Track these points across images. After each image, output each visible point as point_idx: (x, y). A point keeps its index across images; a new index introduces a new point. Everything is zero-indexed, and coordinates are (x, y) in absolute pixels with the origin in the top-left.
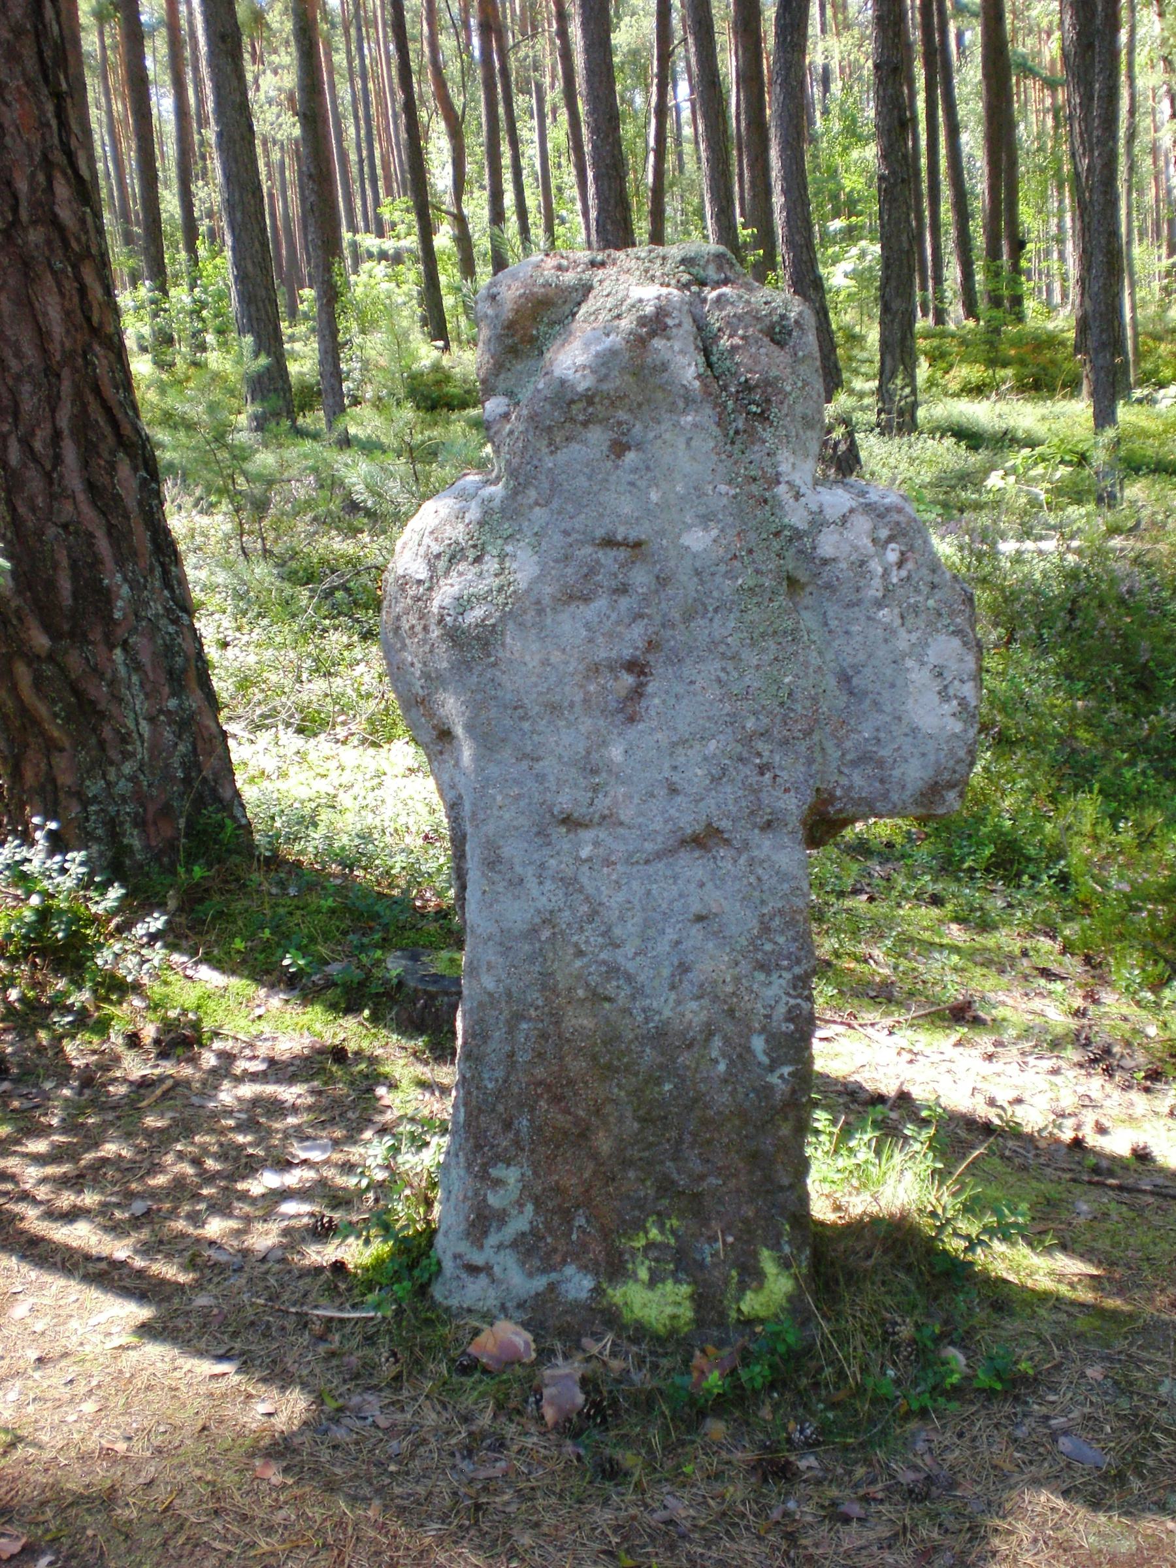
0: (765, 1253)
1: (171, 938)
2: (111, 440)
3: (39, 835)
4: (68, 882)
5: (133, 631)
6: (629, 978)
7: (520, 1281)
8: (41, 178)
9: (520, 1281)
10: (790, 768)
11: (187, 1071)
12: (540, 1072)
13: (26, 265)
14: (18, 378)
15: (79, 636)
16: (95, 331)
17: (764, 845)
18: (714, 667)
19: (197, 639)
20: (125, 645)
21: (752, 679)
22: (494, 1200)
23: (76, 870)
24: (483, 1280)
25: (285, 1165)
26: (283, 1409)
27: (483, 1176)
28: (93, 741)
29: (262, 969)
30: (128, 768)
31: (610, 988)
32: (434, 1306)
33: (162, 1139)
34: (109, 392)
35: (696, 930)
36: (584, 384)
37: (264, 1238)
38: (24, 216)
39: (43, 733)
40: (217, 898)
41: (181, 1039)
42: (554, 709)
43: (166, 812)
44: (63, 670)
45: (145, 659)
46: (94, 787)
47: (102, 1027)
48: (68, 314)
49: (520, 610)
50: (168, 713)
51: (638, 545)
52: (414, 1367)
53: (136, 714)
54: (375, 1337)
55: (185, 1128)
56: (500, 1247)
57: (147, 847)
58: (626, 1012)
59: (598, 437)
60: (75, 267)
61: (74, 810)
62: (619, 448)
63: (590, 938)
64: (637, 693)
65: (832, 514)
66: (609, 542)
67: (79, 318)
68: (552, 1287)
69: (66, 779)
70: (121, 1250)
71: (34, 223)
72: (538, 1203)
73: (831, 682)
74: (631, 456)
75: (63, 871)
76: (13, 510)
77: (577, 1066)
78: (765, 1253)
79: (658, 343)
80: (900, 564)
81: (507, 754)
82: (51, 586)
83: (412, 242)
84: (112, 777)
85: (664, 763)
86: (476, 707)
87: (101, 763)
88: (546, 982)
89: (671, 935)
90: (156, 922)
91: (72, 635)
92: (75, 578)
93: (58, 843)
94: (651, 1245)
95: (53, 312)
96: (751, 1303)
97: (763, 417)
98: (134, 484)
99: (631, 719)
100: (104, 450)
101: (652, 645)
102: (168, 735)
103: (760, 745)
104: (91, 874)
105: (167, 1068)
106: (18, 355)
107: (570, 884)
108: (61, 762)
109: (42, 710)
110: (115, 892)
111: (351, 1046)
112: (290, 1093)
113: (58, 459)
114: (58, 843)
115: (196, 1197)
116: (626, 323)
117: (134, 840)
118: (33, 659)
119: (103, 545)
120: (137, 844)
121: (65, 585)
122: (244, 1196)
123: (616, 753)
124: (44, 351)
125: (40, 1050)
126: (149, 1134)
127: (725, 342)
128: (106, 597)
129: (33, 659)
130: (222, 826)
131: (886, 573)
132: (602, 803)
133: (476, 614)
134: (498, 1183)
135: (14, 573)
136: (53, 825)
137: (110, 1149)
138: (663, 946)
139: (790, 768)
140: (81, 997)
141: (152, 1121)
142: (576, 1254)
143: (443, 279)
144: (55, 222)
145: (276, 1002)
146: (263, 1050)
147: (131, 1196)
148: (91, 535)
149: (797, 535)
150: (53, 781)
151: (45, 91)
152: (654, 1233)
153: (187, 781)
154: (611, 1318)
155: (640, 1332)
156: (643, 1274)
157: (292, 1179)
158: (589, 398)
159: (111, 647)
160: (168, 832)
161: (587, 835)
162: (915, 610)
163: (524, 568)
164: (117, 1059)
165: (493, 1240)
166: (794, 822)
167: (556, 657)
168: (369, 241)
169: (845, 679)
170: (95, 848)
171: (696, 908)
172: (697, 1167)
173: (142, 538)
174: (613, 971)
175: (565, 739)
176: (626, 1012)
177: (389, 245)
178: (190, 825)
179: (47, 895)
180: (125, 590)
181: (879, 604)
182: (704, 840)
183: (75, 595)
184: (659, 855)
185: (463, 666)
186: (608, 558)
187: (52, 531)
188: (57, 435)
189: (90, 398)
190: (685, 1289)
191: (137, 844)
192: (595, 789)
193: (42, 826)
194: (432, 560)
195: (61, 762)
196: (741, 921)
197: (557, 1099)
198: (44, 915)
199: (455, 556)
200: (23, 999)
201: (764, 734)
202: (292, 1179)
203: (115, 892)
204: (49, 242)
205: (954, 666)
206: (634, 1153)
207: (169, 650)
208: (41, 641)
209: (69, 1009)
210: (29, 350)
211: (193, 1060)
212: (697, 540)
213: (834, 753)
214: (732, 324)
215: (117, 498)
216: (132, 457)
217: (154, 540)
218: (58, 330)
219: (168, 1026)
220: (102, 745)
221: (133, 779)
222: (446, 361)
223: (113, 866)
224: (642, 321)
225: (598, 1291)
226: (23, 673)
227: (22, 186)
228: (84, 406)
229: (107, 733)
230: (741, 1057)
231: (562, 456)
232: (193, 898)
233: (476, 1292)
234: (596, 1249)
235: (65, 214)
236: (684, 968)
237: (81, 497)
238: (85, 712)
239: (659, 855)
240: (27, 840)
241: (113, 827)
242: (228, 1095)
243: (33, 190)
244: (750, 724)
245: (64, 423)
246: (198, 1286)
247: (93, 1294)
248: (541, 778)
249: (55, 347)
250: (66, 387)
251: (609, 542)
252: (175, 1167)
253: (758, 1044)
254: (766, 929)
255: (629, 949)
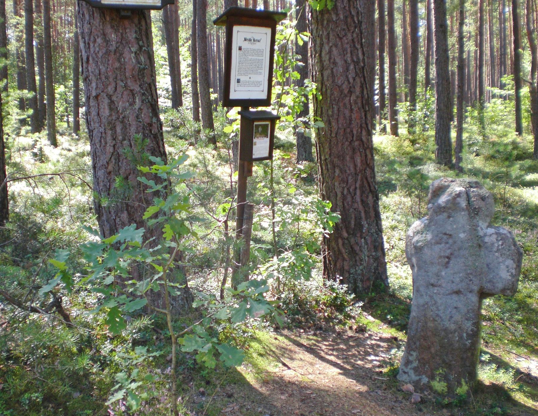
0: (463, 380)
1: (364, 308)
2: (368, 190)
3: (338, 280)
4: (342, 291)
5: (367, 235)
6: (441, 317)
7: (414, 377)
8: (359, 130)
9: (414, 377)
10: (476, 281)
11: (361, 336)
12: (422, 334)
13: (354, 149)
14: (349, 175)
15: (354, 235)
16: (368, 165)
17: (470, 295)
18: (463, 260)
19: (382, 239)
20: (365, 238)
21: (470, 263)
22: (411, 358)
23: (345, 289)
24: (407, 375)
25: (377, 355)
26: (363, 388)
27: (409, 353)
28: (354, 260)
29: (383, 319)
30: (361, 267)
31: (437, 318)
32: (397, 379)
33: (353, 347)
34: (369, 179)
35: (455, 310)
36: (443, 205)
37: (369, 366)
38: (355, 139)
39: (343, 256)
40: (377, 302)
41: (362, 330)
42: (432, 263)
43: (368, 279)
44: (349, 242)
45: (369, 242)
46: (352, 271)
47: (344, 324)
48: (362, 161)
49: (428, 244)
50: (373, 256)
51: (450, 235)
52: (388, 388)
53: (365, 254)
54: (386, 384)
55: (358, 346)
56: (411, 369)
57: (363, 287)
58: (439, 324)
59: (445, 214)
60: (365, 150)
61: (347, 275)
62: (449, 217)
63: (434, 308)
64: (448, 263)
65: (488, 234)
66: (445, 234)
67: (364, 162)
68: (420, 379)
69: (346, 268)
70: (339, 362)
71: (357, 140)
72: (419, 360)
73: (485, 266)
74: (451, 219)
75: (342, 289)
76: (344, 204)
77: (429, 333)
78: (463, 380)
79: (458, 199)
80: (502, 245)
81: (423, 270)
82: (350, 222)
83: (512, 92)
84: (357, 268)
85: (452, 275)
86: (418, 261)
87: (355, 266)
88: (425, 316)
89: (450, 310)
90: (361, 304)
91: (353, 234)
92: (355, 222)
93: (342, 282)
94: (440, 373)
95: (358, 160)
96: (459, 391)
97: (477, 214)
98: (372, 201)
99: (447, 267)
100: (366, 192)
101: (451, 254)
102: (372, 261)
103: (470, 276)
104: (348, 290)
105: (357, 335)
106: (349, 170)
107: (431, 297)
108: (346, 263)
109: (343, 251)
110: (353, 296)
111: (400, 338)
112: (382, 344)
113: (355, 194)
114: (342, 282)
115: (356, 357)
116: (453, 194)
117: (360, 285)
118: (343, 239)
119: (363, 215)
120: (360, 286)
121: (353, 223)
122: (367, 359)
123: (443, 273)
124: (355, 169)
125: (330, 326)
126: (350, 345)
127: (473, 199)
128: (362, 226)
129: (343, 239)
130: (381, 285)
131: (498, 246)
132: (439, 282)
133: (420, 244)
134: (412, 355)
135: (342, 219)
136: (341, 278)
137: (341, 346)
138: (448, 312)
139: (476, 281)
140: (341, 317)
141: (351, 343)
142: (425, 373)
143: (523, 107)
144: (361, 140)
145: (385, 326)
146: (379, 335)
147: (343, 354)
148: (360, 212)
149: (481, 237)
150: (343, 267)
151: (363, 110)
152: (441, 371)
153: (375, 273)
154: (431, 388)
155: (436, 392)
156: (438, 380)
157: (377, 358)
158: (444, 207)
159: (361, 238)
160: (368, 284)
161: (436, 288)
162: (504, 254)
163: (429, 237)
164: (346, 331)
165: (409, 367)
166: (476, 291)
167: (433, 254)
168: (497, 91)
169: (488, 265)
170: (350, 285)
171: (455, 305)
172: (451, 358)
173: (372, 214)
174: (437, 315)
175: (434, 269)
176: (439, 324)
177: (503, 92)
178: (373, 283)
179: (337, 294)
180: (367, 226)
181: (496, 252)
182: (458, 292)
183: (355, 225)
184: (449, 294)
185: (416, 253)
186: (445, 237)
187: (351, 210)
188: (356, 188)
189: (365, 180)
190: (446, 384)
191: (360, 286)
192: (439, 280)
193: (339, 278)
194: (414, 233)
195: (346, 263)
196: (464, 310)
197: (425, 340)
198: (336, 298)
199: (418, 232)
200: (328, 315)
201: (471, 274)
202: (377, 358)
203: (353, 296)
204: (360, 145)
205: (511, 266)
206: (438, 353)
207: (375, 241)
208: (345, 235)
209: (337, 319)
210: (352, 169)
211: (363, 334)
212: (462, 235)
213: (485, 279)
214: (475, 196)
215: (368, 204)
216: (373, 194)
217: (375, 214)
218: (359, 165)
219: (359, 327)
220: (356, 261)
221: (362, 270)
222: (519, 140)
223: (354, 289)
224: (456, 195)
225: (429, 382)
226: (340, 241)
227: (355, 132)
228: (363, 183)
229: (357, 258)
230: (461, 337)
231: (438, 217)
232: (371, 300)
233: (404, 377)
234: (429, 373)
235: (364, 139)
236: (451, 317)
237: (359, 203)
238: (353, 253)
239: (449, 294)
240: (335, 280)
241: (355, 283)
242: (369, 342)
243: (357, 133)
244: (469, 272)
245: (358, 186)
246: (352, 370)
247: (331, 367)
248: (428, 276)
249: (358, 169)
250: (359, 177)
251: (445, 234)
252: (354, 351)
253: (465, 335)
254: (468, 312)
255: (441, 311)
